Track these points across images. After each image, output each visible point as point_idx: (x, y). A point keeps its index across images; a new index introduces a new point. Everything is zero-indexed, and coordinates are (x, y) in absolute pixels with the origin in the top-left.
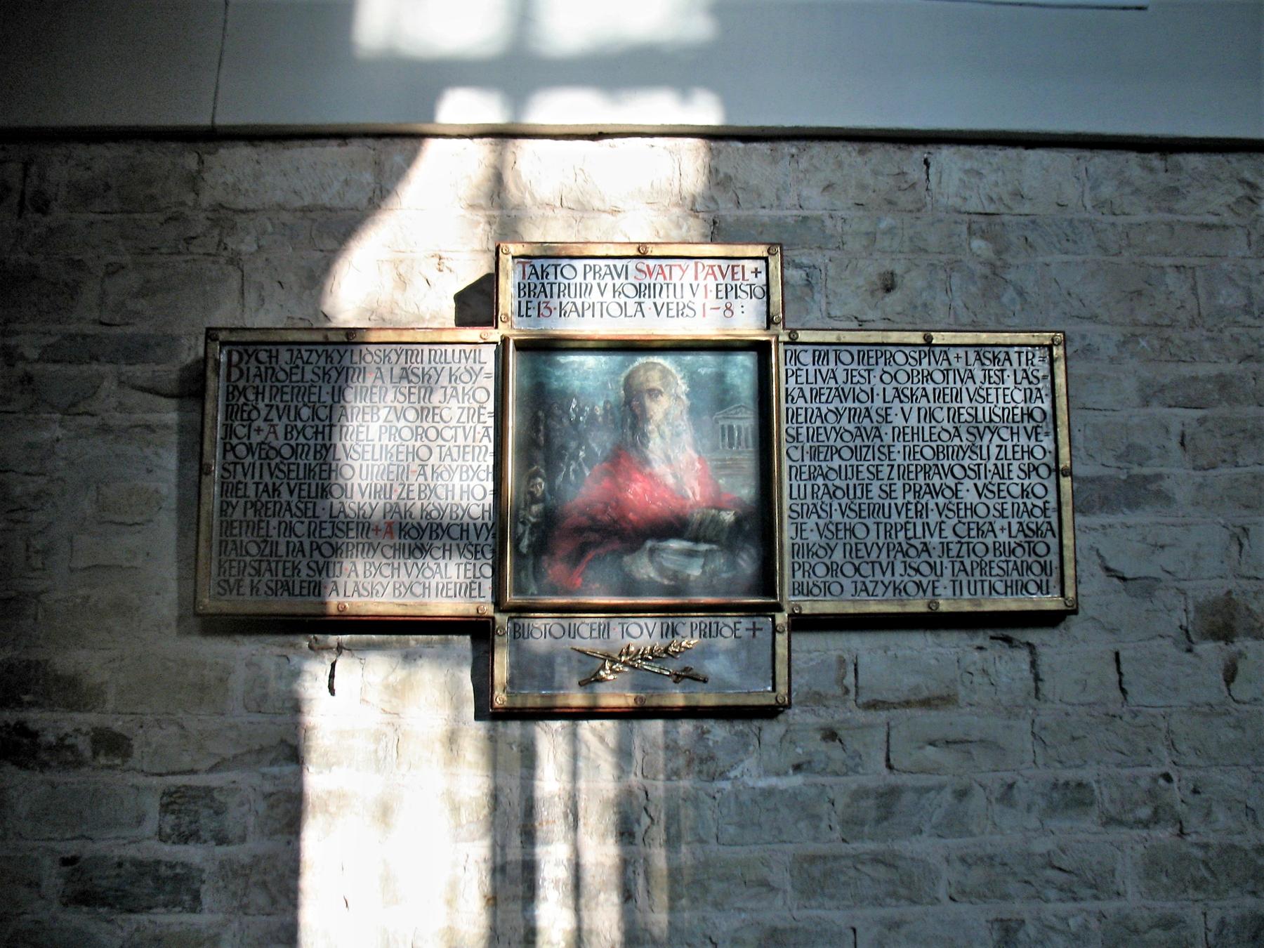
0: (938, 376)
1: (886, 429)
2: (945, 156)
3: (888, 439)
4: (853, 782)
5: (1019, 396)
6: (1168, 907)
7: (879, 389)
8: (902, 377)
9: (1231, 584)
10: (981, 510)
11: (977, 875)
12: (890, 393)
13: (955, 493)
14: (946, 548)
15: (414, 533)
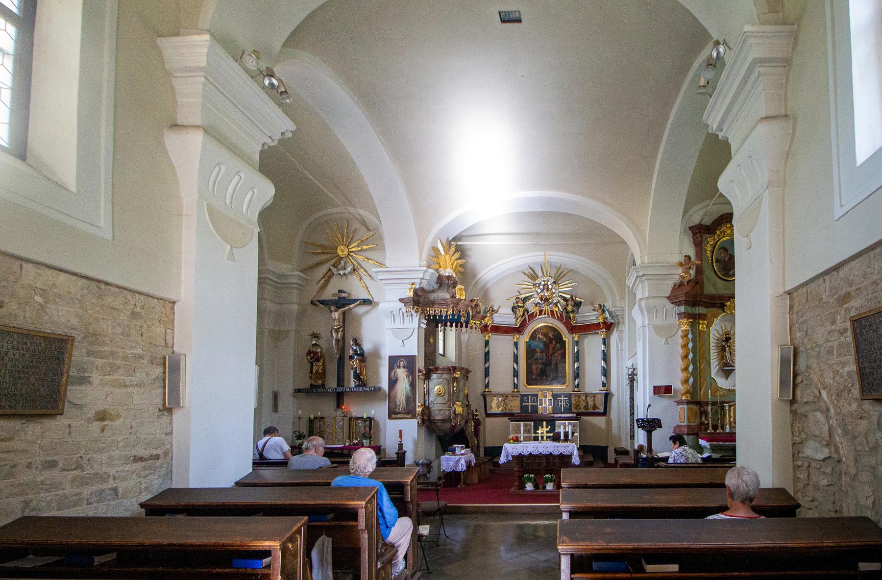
0: (29, 344)
1: (6, 358)
2: (63, 275)
3: (6, 361)
5: (56, 353)
6: (77, 491)
7: (6, 345)
8: (15, 342)
9: (107, 407)
10: (36, 385)
12: (10, 347)
13: (28, 379)
14: (22, 395)
15: (318, 367)
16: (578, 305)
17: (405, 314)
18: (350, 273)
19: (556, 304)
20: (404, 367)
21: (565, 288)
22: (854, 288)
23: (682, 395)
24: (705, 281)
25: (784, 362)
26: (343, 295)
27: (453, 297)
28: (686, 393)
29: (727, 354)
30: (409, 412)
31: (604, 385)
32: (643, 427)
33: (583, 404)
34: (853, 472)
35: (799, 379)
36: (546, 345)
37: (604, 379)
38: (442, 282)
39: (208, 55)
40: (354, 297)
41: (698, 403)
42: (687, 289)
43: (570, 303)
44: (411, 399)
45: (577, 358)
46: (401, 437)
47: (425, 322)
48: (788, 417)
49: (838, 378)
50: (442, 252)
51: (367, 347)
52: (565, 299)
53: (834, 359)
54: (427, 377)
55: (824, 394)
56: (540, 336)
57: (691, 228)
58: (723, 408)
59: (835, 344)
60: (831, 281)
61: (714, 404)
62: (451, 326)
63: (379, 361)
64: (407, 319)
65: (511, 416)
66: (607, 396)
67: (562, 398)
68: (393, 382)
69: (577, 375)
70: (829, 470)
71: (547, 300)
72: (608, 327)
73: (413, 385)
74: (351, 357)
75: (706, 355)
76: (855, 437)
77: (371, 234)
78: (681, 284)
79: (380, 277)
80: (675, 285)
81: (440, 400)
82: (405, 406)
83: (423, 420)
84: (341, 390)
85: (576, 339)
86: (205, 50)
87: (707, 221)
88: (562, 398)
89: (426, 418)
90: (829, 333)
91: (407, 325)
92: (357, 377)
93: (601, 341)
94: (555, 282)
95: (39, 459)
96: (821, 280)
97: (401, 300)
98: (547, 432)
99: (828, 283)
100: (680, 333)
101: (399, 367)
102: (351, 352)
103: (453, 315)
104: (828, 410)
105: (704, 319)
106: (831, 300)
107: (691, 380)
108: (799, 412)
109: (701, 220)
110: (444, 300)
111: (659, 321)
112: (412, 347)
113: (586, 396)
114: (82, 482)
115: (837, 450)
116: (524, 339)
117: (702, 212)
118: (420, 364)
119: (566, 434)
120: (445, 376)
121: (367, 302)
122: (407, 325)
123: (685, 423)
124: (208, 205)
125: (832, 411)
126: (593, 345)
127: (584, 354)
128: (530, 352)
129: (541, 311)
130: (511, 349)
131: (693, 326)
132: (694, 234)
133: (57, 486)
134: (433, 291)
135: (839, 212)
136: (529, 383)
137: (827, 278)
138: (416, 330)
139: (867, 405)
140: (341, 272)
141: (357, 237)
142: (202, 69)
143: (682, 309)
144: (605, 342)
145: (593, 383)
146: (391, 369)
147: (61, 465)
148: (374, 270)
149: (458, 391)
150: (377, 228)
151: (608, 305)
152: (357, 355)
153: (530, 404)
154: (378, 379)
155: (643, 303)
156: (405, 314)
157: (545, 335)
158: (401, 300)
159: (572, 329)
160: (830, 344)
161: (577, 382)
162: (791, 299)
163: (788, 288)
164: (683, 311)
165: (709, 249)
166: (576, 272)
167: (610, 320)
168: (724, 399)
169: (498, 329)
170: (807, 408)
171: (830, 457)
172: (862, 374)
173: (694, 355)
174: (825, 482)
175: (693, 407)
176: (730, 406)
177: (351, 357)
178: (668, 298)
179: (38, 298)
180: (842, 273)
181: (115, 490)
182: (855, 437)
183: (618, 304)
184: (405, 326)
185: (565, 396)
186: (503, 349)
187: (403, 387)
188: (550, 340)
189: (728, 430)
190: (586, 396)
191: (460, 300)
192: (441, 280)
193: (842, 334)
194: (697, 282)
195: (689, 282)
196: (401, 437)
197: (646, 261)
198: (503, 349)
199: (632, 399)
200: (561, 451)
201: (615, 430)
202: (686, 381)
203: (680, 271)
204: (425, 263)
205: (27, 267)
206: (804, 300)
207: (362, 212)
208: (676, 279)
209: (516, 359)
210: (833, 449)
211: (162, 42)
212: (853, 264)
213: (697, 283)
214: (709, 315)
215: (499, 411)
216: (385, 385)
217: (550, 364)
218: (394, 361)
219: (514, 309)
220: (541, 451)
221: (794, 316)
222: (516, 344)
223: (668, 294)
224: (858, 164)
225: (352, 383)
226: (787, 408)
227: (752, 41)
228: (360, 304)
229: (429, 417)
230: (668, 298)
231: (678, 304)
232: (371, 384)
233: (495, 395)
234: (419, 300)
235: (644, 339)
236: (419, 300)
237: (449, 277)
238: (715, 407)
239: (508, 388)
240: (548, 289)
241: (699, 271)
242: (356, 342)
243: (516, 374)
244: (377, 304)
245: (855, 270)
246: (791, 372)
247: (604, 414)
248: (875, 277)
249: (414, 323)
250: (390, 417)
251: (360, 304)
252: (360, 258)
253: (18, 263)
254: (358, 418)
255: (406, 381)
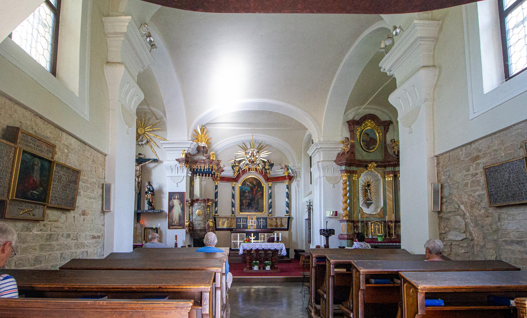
4: (47, 233)
6: (76, 250)
11: (59, 247)
16: (272, 165)
17: (179, 168)
18: (145, 144)
19: (258, 164)
20: (178, 199)
21: (264, 155)
22: (482, 153)
23: (344, 217)
24: (356, 152)
25: (435, 192)
26: (141, 156)
27: (209, 158)
28: (345, 216)
29: (369, 194)
30: (181, 225)
31: (287, 212)
32: (324, 234)
33: (279, 223)
34: (482, 244)
35: (444, 200)
36: (252, 189)
37: (287, 209)
38: (199, 149)
39: (128, 27)
40: (147, 158)
41: (353, 222)
42: (347, 156)
43: (267, 164)
44: (181, 218)
45: (270, 196)
46: (176, 239)
47: (191, 173)
48: (437, 220)
49: (471, 198)
50: (200, 133)
51: (155, 186)
52: (264, 162)
53: (469, 188)
54: (192, 205)
55: (462, 207)
56: (248, 183)
57: (347, 122)
58: (367, 224)
59: (469, 181)
60: (466, 150)
61: (362, 222)
62: (206, 176)
63: (162, 195)
64: (179, 171)
65: (230, 230)
66: (289, 219)
67: (262, 220)
68: (171, 208)
69: (270, 207)
70: (465, 245)
71: (253, 162)
72: (290, 178)
73: (183, 209)
74: (146, 193)
75: (357, 193)
76: (483, 227)
77: (158, 121)
78: (343, 153)
79: (164, 146)
80: (339, 154)
81: (199, 218)
82: (178, 221)
83: (189, 230)
84: (140, 211)
85: (270, 185)
86: (127, 24)
87: (357, 118)
88: (262, 220)
89: (191, 228)
90: (465, 176)
91: (179, 174)
92: (150, 204)
93: (285, 187)
94: (258, 152)
95: (65, 233)
96: (460, 149)
97: (177, 160)
98: (254, 240)
99: (464, 151)
100: (342, 181)
101: (175, 199)
102: (147, 190)
103: (209, 169)
104: (464, 215)
105: (355, 174)
106: (466, 159)
107: (348, 209)
108: (444, 217)
109: (354, 117)
110: (204, 160)
111: (329, 174)
112: (183, 188)
113: (276, 219)
114: (78, 246)
115: (471, 234)
116: (239, 185)
117: (354, 113)
118: (187, 197)
119: (278, 238)
120: (202, 204)
121: (155, 161)
122: (179, 174)
123: (346, 233)
124: (122, 105)
125: (468, 214)
126: (280, 189)
127: (274, 194)
128: (242, 193)
129: (249, 169)
130: (229, 191)
131: (349, 177)
132: (350, 125)
133: (69, 247)
134: (194, 155)
135: (472, 116)
136: (241, 211)
137: (464, 148)
138: (185, 177)
139: (491, 210)
140: (140, 143)
141: (150, 122)
142: (125, 34)
143: (343, 168)
144: (288, 187)
145: (280, 211)
146: (170, 199)
147: (72, 236)
148: (161, 142)
149: (210, 213)
150: (162, 118)
151: (291, 165)
152: (151, 191)
153: (242, 223)
154: (161, 205)
155: (320, 164)
156: (179, 168)
157: (251, 183)
158: (177, 160)
159: (268, 179)
160: (466, 181)
161: (270, 211)
162: (437, 160)
163: (436, 154)
164: (344, 169)
165: (358, 134)
166: (271, 146)
167: (292, 175)
168: (367, 219)
169: (223, 179)
170: (450, 214)
171: (466, 238)
172: (490, 195)
173: (350, 195)
174: (463, 251)
175: (350, 223)
176: (372, 223)
177: (146, 193)
178: (335, 161)
179: (66, 150)
180: (473, 146)
181: (87, 252)
182: (483, 227)
183: (296, 165)
184: (179, 174)
185: (263, 218)
186: (226, 191)
187: (177, 210)
188: (255, 186)
189: (370, 237)
190: (276, 219)
191: (213, 160)
192: (199, 149)
193: (474, 176)
194: (352, 151)
195: (347, 152)
196: (176, 239)
197: (322, 140)
198: (226, 191)
199: (309, 220)
200: (276, 248)
201: (294, 239)
202: (346, 209)
203: (342, 146)
204: (190, 139)
205: (64, 134)
206: (447, 160)
207: (153, 109)
208: (340, 151)
209: (233, 196)
210: (468, 234)
211: (104, 19)
212: (481, 141)
213: (352, 153)
214: (358, 172)
215: (225, 226)
216: (166, 209)
217: (254, 200)
218: (171, 195)
219: (233, 167)
220: (263, 247)
221: (440, 168)
222: (233, 188)
223: (335, 159)
224: (485, 93)
225: (146, 207)
226: (436, 215)
227: (417, 28)
228: (152, 162)
229: (193, 228)
230: (335, 161)
231: (341, 165)
232: (157, 208)
233: (221, 218)
234: (188, 160)
235: (320, 185)
236: (188, 160)
237: (204, 147)
238: (363, 224)
239: (229, 214)
240: (254, 156)
241: (353, 146)
242: (150, 184)
243: (233, 205)
244: (162, 162)
245: (483, 144)
246: (440, 197)
247: (287, 229)
248: (495, 148)
249: (184, 173)
250: (169, 228)
251: (152, 162)
252: (151, 135)
253: (61, 132)
254: (150, 228)
255: (179, 207)
